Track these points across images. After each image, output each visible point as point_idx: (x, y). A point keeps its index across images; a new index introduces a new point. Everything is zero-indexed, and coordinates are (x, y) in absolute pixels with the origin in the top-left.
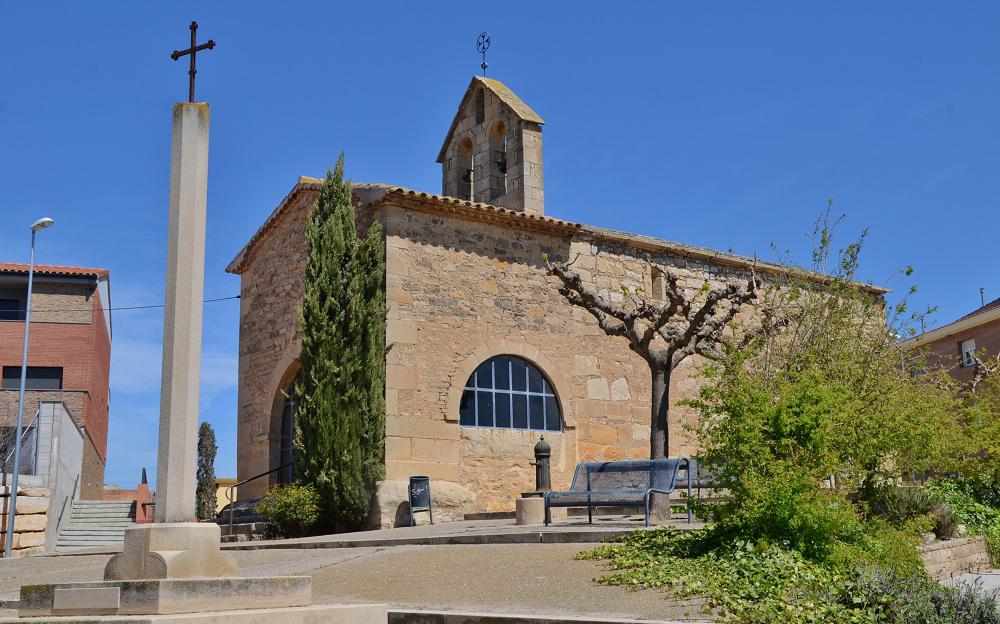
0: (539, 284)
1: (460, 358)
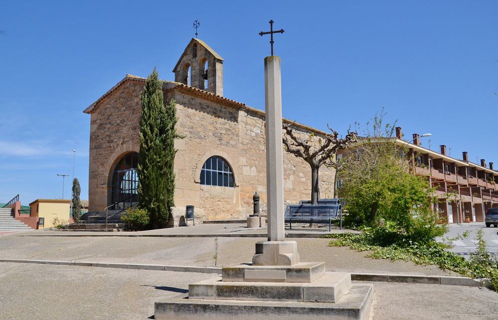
0: (228, 127)
1: (200, 156)
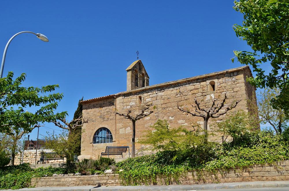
0: (108, 110)
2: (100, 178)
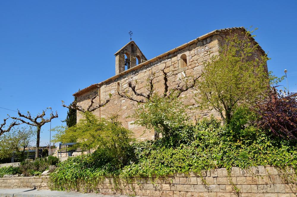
2: (35, 179)
